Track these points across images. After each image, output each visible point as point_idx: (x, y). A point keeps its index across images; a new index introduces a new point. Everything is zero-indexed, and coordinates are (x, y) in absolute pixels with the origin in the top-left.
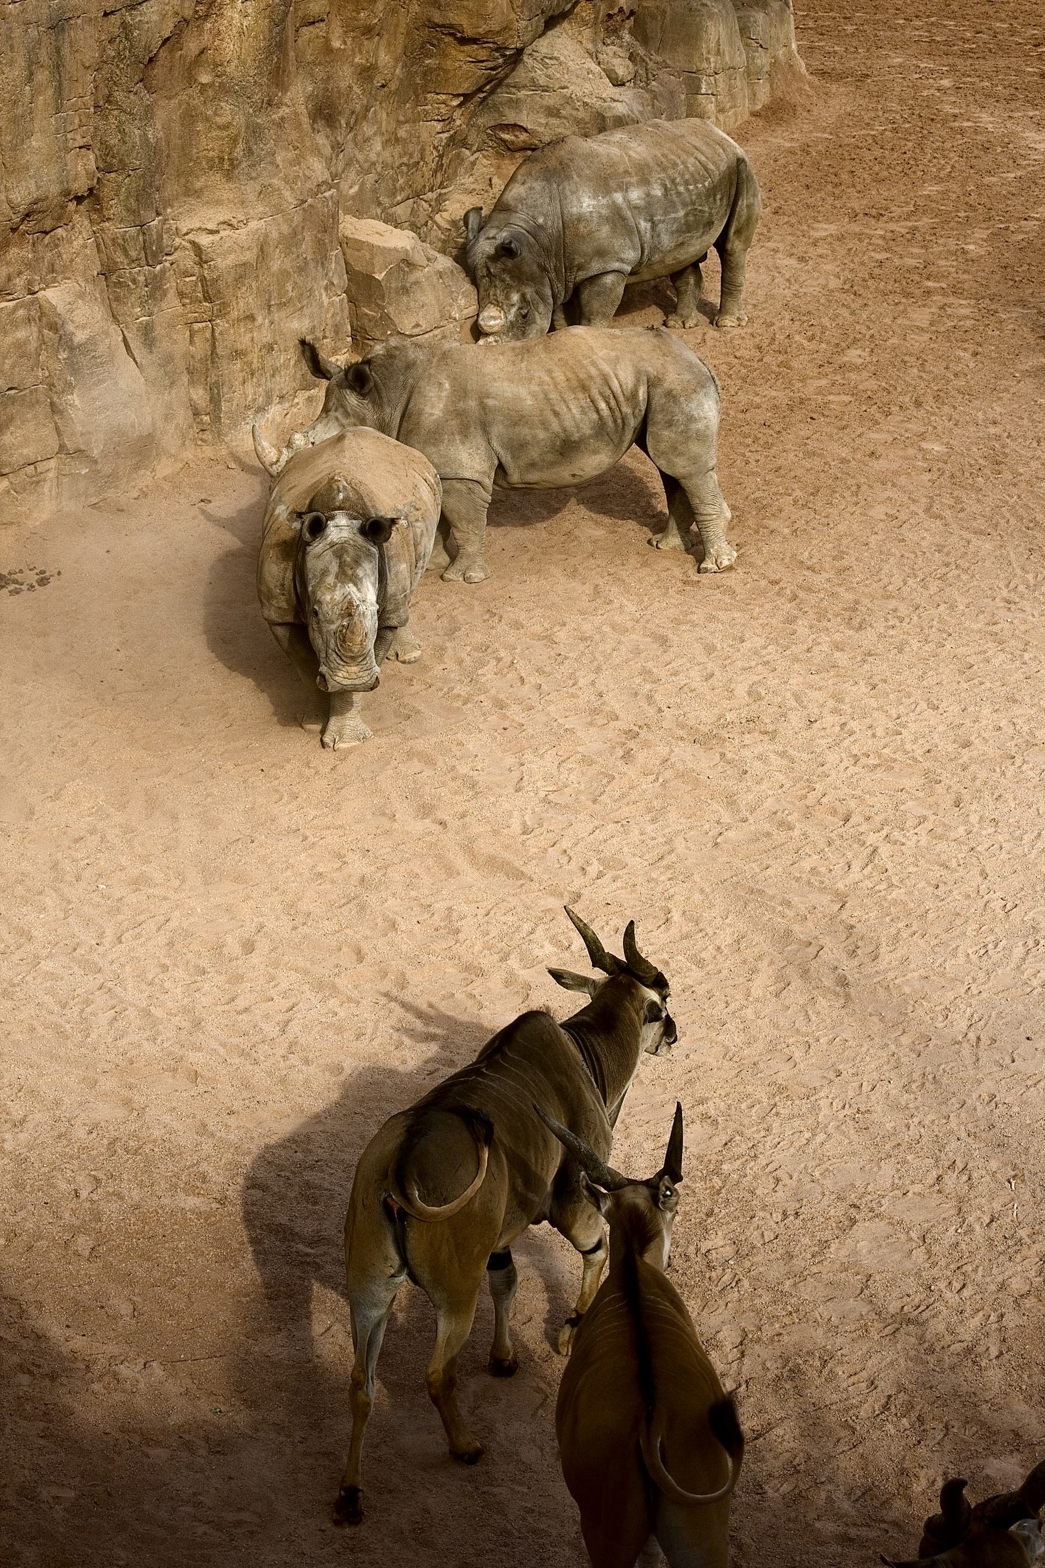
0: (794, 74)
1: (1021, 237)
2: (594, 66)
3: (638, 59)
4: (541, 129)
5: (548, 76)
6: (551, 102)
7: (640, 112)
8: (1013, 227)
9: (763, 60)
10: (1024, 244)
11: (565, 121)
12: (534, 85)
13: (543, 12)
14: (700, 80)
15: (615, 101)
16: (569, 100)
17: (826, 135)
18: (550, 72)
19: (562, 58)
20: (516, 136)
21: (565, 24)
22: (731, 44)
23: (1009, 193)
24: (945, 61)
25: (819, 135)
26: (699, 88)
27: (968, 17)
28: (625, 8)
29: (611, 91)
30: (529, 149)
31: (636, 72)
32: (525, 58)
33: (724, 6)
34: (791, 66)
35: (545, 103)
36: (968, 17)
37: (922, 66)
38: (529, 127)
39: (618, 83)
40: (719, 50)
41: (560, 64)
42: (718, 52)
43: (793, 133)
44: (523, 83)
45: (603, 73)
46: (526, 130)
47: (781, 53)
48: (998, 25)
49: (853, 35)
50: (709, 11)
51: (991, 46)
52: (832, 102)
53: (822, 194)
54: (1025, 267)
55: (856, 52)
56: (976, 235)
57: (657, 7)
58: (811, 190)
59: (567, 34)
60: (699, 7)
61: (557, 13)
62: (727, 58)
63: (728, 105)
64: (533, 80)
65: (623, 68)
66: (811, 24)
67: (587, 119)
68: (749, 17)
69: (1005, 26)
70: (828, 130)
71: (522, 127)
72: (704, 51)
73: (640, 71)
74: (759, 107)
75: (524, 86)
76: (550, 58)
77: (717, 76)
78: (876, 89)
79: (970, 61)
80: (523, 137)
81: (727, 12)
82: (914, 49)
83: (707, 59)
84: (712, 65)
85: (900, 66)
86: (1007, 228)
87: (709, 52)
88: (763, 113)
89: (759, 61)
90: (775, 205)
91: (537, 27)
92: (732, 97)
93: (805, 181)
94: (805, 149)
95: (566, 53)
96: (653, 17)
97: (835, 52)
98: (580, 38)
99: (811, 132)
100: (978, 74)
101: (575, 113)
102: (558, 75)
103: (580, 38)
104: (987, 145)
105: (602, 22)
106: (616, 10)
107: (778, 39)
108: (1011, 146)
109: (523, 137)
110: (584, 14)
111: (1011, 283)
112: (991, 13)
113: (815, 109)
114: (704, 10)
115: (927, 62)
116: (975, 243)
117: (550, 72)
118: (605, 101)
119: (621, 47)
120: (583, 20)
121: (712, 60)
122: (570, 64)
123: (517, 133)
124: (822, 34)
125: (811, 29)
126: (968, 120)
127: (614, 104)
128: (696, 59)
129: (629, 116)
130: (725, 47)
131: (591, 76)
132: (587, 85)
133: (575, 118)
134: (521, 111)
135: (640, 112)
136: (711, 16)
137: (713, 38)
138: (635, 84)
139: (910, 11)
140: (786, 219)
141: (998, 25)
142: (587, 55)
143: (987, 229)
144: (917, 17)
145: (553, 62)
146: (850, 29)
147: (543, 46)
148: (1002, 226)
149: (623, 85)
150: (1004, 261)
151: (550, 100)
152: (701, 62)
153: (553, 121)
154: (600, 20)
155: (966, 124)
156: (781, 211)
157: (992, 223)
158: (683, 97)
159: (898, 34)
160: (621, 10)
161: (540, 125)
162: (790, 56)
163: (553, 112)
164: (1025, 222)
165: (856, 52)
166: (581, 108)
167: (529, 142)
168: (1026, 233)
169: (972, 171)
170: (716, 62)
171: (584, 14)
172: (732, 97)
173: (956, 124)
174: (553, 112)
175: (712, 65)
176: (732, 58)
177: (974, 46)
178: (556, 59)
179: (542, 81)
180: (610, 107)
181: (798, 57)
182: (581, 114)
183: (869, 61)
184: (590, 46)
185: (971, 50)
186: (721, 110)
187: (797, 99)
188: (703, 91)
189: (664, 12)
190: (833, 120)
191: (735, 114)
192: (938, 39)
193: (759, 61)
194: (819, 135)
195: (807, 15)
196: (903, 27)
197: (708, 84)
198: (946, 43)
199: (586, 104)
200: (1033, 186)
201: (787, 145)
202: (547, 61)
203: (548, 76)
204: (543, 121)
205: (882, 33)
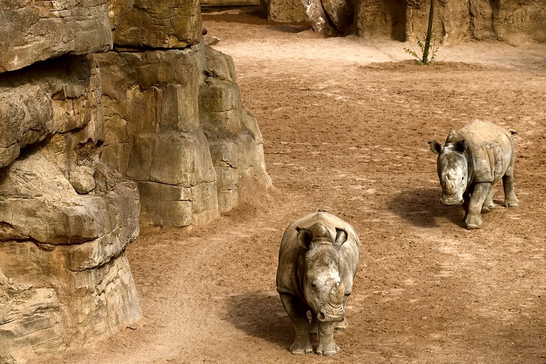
0: (258, 186)
1: (388, 299)
2: (64, 180)
3: (100, 175)
4: (22, 226)
5: (27, 187)
6: (30, 206)
7: (95, 213)
8: (384, 293)
9: (232, 176)
10: (388, 304)
11: (39, 219)
12: (18, 194)
13: (18, 142)
14: (180, 191)
15: (76, 205)
16: (42, 204)
17: (273, 229)
18: (29, 184)
19: (38, 175)
20: (4, 230)
21: (44, 151)
22: (204, 164)
23: (390, 269)
24: (375, 176)
25: (268, 229)
26: (179, 196)
27: (402, 145)
28: (93, 139)
29: (76, 198)
30: (15, 240)
31: (97, 185)
32: (11, 175)
33: (198, 137)
34: (256, 180)
35: (25, 206)
36: (402, 145)
37: (357, 179)
38: (14, 224)
39: (81, 191)
40: (194, 169)
41: (37, 179)
42: (193, 171)
43: (250, 228)
44: (9, 193)
45: (70, 185)
46: (11, 226)
47: (248, 172)
48: (422, 150)
49: (316, 158)
50: (186, 142)
51: (412, 165)
52: (284, 206)
53: (256, 271)
54: (383, 321)
55: (315, 170)
56: (357, 299)
57: (149, 139)
58: (249, 268)
59: (46, 157)
60: (179, 139)
61: (32, 142)
62: (201, 175)
63: (201, 208)
64: (16, 190)
65: (86, 182)
66: (289, 151)
67: (56, 218)
68: (221, 145)
69: (426, 151)
70: (276, 225)
71: (8, 224)
72: (183, 170)
73: (100, 184)
74: (229, 209)
75: (10, 195)
76: (30, 175)
77: (193, 188)
78: (321, 196)
79: (393, 176)
80: (9, 231)
81: (200, 142)
82: (356, 167)
83: (185, 176)
84: (189, 180)
85: (343, 179)
86: (380, 294)
87: (186, 171)
88: (231, 214)
89: (229, 177)
90: (220, 278)
91: (14, 152)
92: (205, 202)
93: (246, 261)
94: (254, 239)
95: (42, 171)
96: (146, 146)
97: (299, 170)
98: (55, 159)
99: (263, 227)
100: (395, 185)
101: (47, 213)
102: (35, 187)
103: (55, 160)
104: (385, 235)
105: (75, 149)
106: (86, 140)
107: (245, 162)
108: (402, 235)
109: (9, 231)
110: (58, 143)
111: (370, 333)
112: (419, 141)
113: (270, 210)
114: (182, 140)
115: (362, 177)
116: (353, 305)
117: (29, 184)
118: (69, 205)
119: (90, 166)
120: (57, 147)
121: (188, 176)
122: (45, 178)
123: (5, 228)
124: (294, 158)
125: (287, 154)
126: (378, 217)
127: (76, 207)
128: (177, 176)
129: (86, 216)
130: (199, 167)
131: (60, 187)
132: (57, 194)
133: (47, 218)
134: (7, 212)
135: (95, 213)
136: (187, 145)
137: (189, 161)
138: (96, 193)
139: (362, 141)
140: (225, 289)
141: (422, 150)
142: (60, 172)
143: (366, 294)
144: (366, 145)
145: (31, 177)
146: (315, 153)
147: (25, 166)
148: (377, 292)
149: (87, 193)
150: (370, 317)
151: (29, 204)
152: (181, 177)
153: (31, 219)
154: (73, 147)
155: (375, 220)
156: (222, 283)
157: (370, 290)
158: (137, 202)
159: (348, 157)
160: (90, 140)
161: (21, 222)
162: (257, 173)
163: (31, 213)
164: (394, 289)
165: (315, 170)
166: (51, 211)
167: (14, 235)
168: (393, 297)
169: (369, 253)
170: (191, 178)
171: (58, 143)
172: (205, 202)
173: (368, 220)
174: (31, 213)
175: (189, 180)
176: (204, 174)
177: (400, 165)
178: (34, 175)
179: (23, 191)
180: (72, 210)
181: (267, 174)
182: (51, 215)
183: (322, 177)
184: (63, 166)
185: (397, 169)
186: (196, 212)
187: (258, 202)
188: (182, 198)
189: (154, 142)
190: (281, 218)
191: (207, 215)
192: (376, 160)
193: (229, 177)
194: (268, 229)
195: (287, 145)
196: (353, 152)
197: (186, 193)
198: (382, 164)
199: (55, 207)
200: (408, 263)
201: (243, 236)
202: (28, 176)
203: (27, 187)
204: (24, 219)
205: (337, 156)
